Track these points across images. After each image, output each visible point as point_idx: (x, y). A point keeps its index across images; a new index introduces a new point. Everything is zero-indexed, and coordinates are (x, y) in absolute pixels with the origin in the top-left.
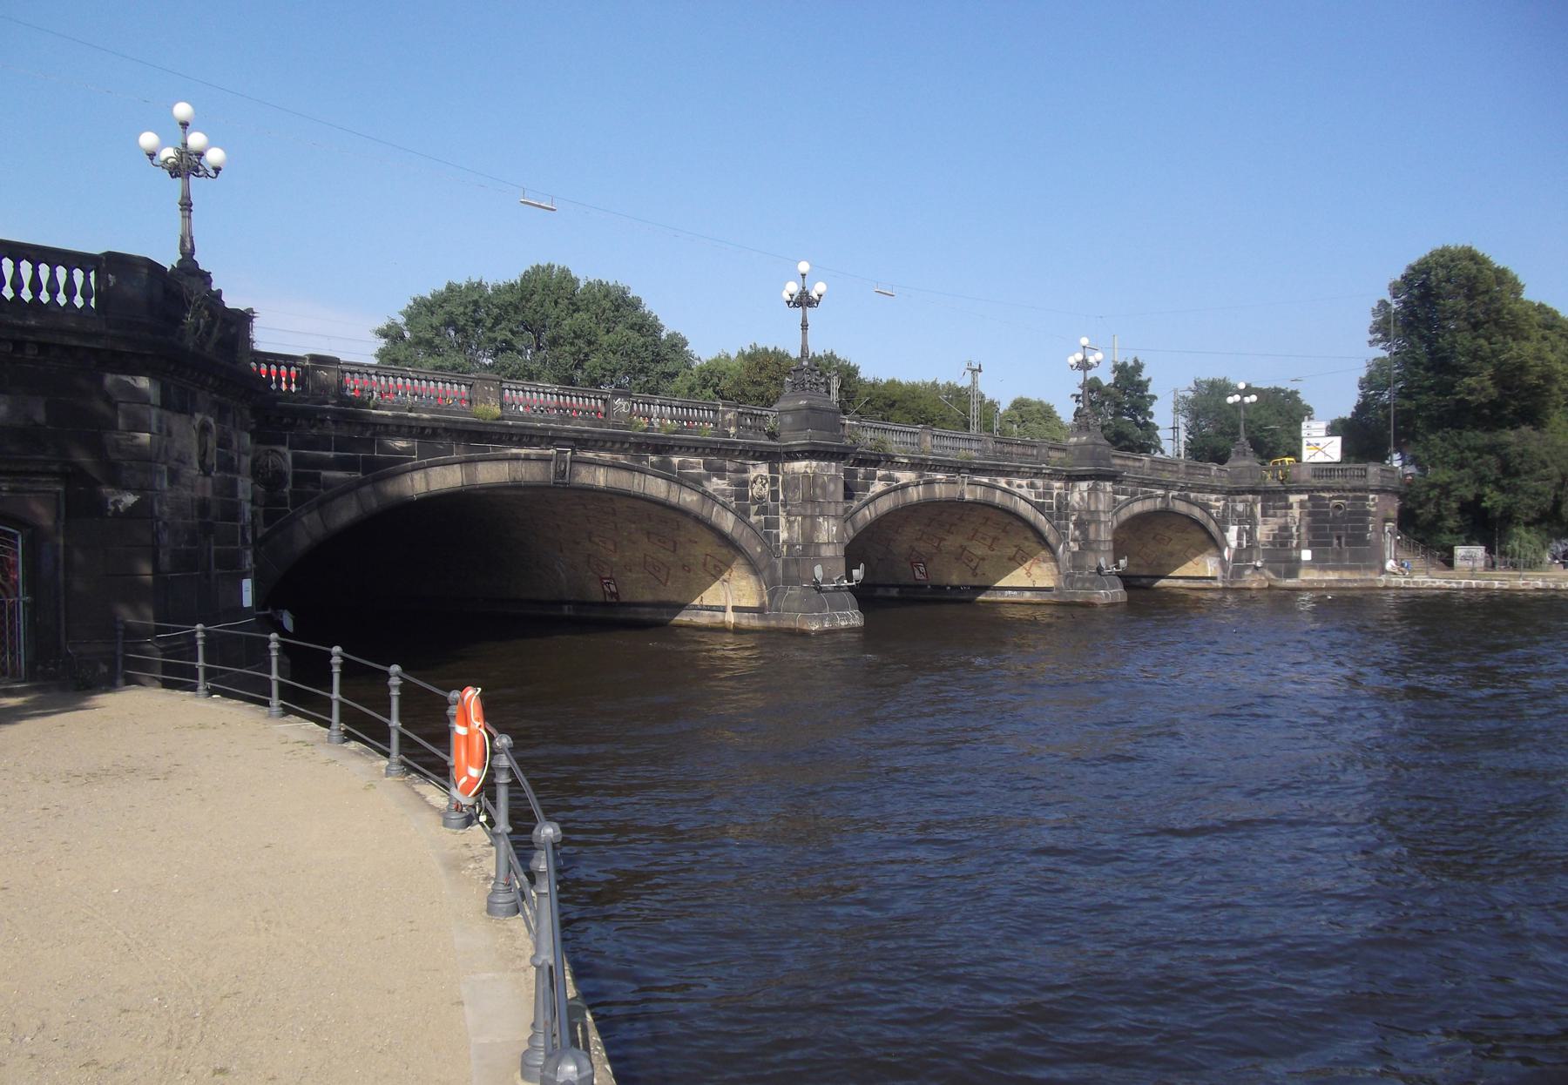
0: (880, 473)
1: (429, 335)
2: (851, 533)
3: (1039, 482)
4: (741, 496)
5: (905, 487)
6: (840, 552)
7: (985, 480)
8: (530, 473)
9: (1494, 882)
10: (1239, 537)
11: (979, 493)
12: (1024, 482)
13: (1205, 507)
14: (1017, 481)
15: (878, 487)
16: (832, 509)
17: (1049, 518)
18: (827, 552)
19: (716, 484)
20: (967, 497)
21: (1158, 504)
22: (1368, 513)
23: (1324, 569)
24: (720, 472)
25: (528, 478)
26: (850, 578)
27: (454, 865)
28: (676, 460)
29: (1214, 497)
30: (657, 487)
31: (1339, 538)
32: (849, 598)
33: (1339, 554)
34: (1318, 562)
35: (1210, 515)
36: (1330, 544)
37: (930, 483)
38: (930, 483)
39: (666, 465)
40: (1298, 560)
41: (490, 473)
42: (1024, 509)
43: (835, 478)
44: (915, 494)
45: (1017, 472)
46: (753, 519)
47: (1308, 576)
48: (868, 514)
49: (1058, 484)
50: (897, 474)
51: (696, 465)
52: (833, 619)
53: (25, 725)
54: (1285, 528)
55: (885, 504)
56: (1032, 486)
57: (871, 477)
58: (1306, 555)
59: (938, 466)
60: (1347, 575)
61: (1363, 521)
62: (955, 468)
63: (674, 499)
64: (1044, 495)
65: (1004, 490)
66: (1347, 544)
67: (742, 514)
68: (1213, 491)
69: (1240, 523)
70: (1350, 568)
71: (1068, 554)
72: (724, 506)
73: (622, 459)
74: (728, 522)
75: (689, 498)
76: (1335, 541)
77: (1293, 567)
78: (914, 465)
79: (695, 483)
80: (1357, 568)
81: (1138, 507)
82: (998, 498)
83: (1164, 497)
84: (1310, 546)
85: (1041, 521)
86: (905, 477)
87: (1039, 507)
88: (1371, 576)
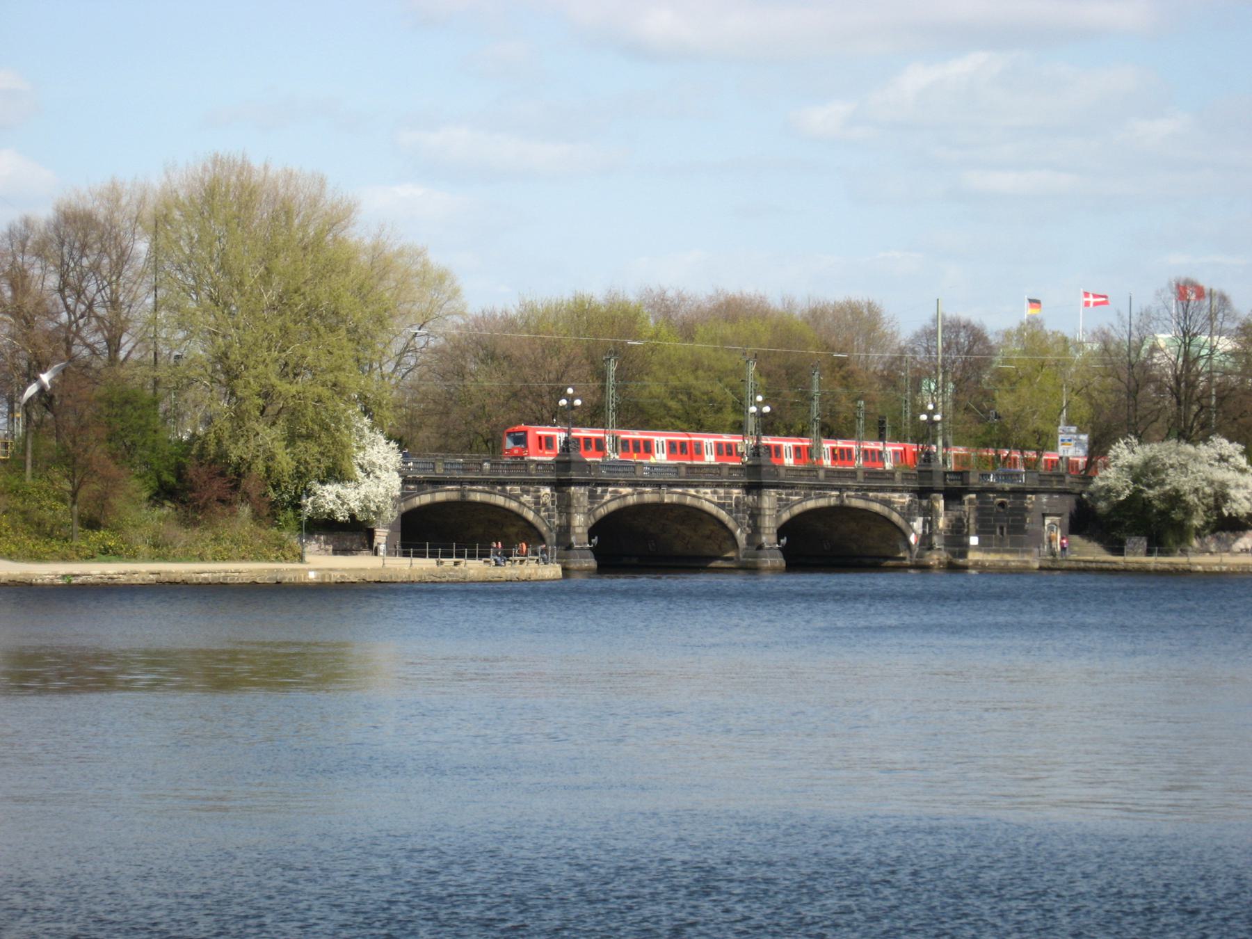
0: (610, 489)
2: (593, 521)
3: (721, 491)
4: (537, 503)
5: (625, 496)
6: (586, 530)
7: (680, 490)
8: (454, 496)
9: (470, 900)
10: (924, 526)
11: (675, 498)
12: (709, 491)
14: (703, 490)
15: (608, 497)
17: (730, 513)
18: (579, 530)
19: (526, 498)
21: (833, 501)
22: (1026, 509)
23: (988, 552)
24: (527, 492)
26: (779, 543)
27: (497, 564)
28: (508, 488)
30: (500, 500)
31: (1002, 528)
32: (590, 553)
33: (1001, 540)
34: (983, 546)
35: (894, 510)
36: (994, 532)
37: (641, 493)
38: (641, 493)
39: (504, 491)
41: (440, 497)
42: (713, 509)
43: (583, 494)
44: (632, 500)
45: (704, 485)
46: (542, 514)
47: (973, 556)
48: (602, 511)
50: (621, 490)
51: (517, 489)
54: (959, 520)
55: (613, 506)
56: (715, 493)
57: (605, 492)
58: (974, 541)
60: (1008, 557)
61: (1022, 515)
62: (658, 485)
63: (507, 505)
65: (693, 496)
66: (1009, 533)
67: (537, 512)
69: (924, 515)
70: (1010, 552)
73: (486, 488)
74: (530, 516)
75: (513, 505)
76: (998, 530)
78: (630, 484)
79: (516, 498)
80: (1016, 552)
81: (811, 504)
82: (688, 500)
83: (838, 497)
84: (978, 533)
87: (722, 506)
88: (1026, 558)
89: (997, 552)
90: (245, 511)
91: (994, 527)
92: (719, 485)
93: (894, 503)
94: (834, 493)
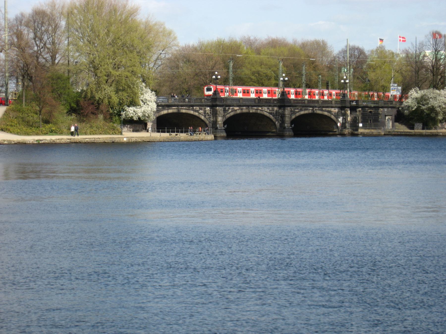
0: (231, 108)
1: (181, 83)
3: (271, 108)
4: (205, 113)
5: (236, 110)
8: (175, 111)
11: (254, 111)
12: (266, 108)
13: (330, 112)
15: (230, 111)
16: (221, 115)
17: (273, 116)
18: (220, 123)
19: (201, 111)
20: (251, 112)
22: (379, 114)
23: (365, 129)
24: (201, 109)
25: (254, 220)
28: (195, 108)
29: (333, 109)
30: (192, 112)
31: (370, 120)
32: (224, 131)
34: (364, 127)
35: (332, 114)
36: (368, 122)
37: (242, 109)
38: (242, 109)
40: (358, 126)
41: (170, 111)
42: (266, 114)
44: (239, 112)
45: (264, 106)
46: (207, 117)
47: (360, 131)
48: (228, 116)
49: (276, 108)
50: (235, 108)
51: (198, 108)
52: (360, 95)
53: (270, 140)
54: (355, 118)
55: (232, 114)
56: (268, 109)
57: (229, 109)
58: (361, 125)
59: (244, 106)
60: (373, 131)
61: (378, 116)
63: (194, 114)
64: (272, 111)
65: (260, 110)
67: (205, 116)
68: (332, 107)
69: (343, 116)
71: (279, 124)
72: (202, 115)
73: (187, 108)
74: (203, 118)
75: (196, 114)
76: (369, 121)
77: (357, 128)
78: (238, 106)
79: (197, 111)
80: (376, 129)
81: (302, 113)
82: (259, 111)
83: (312, 110)
84: (362, 122)
85: (271, 117)
86: (236, 108)
89: (369, 129)
90: (101, 117)
91: (368, 120)
92: (270, 106)
93: (332, 112)
94: (311, 108)
